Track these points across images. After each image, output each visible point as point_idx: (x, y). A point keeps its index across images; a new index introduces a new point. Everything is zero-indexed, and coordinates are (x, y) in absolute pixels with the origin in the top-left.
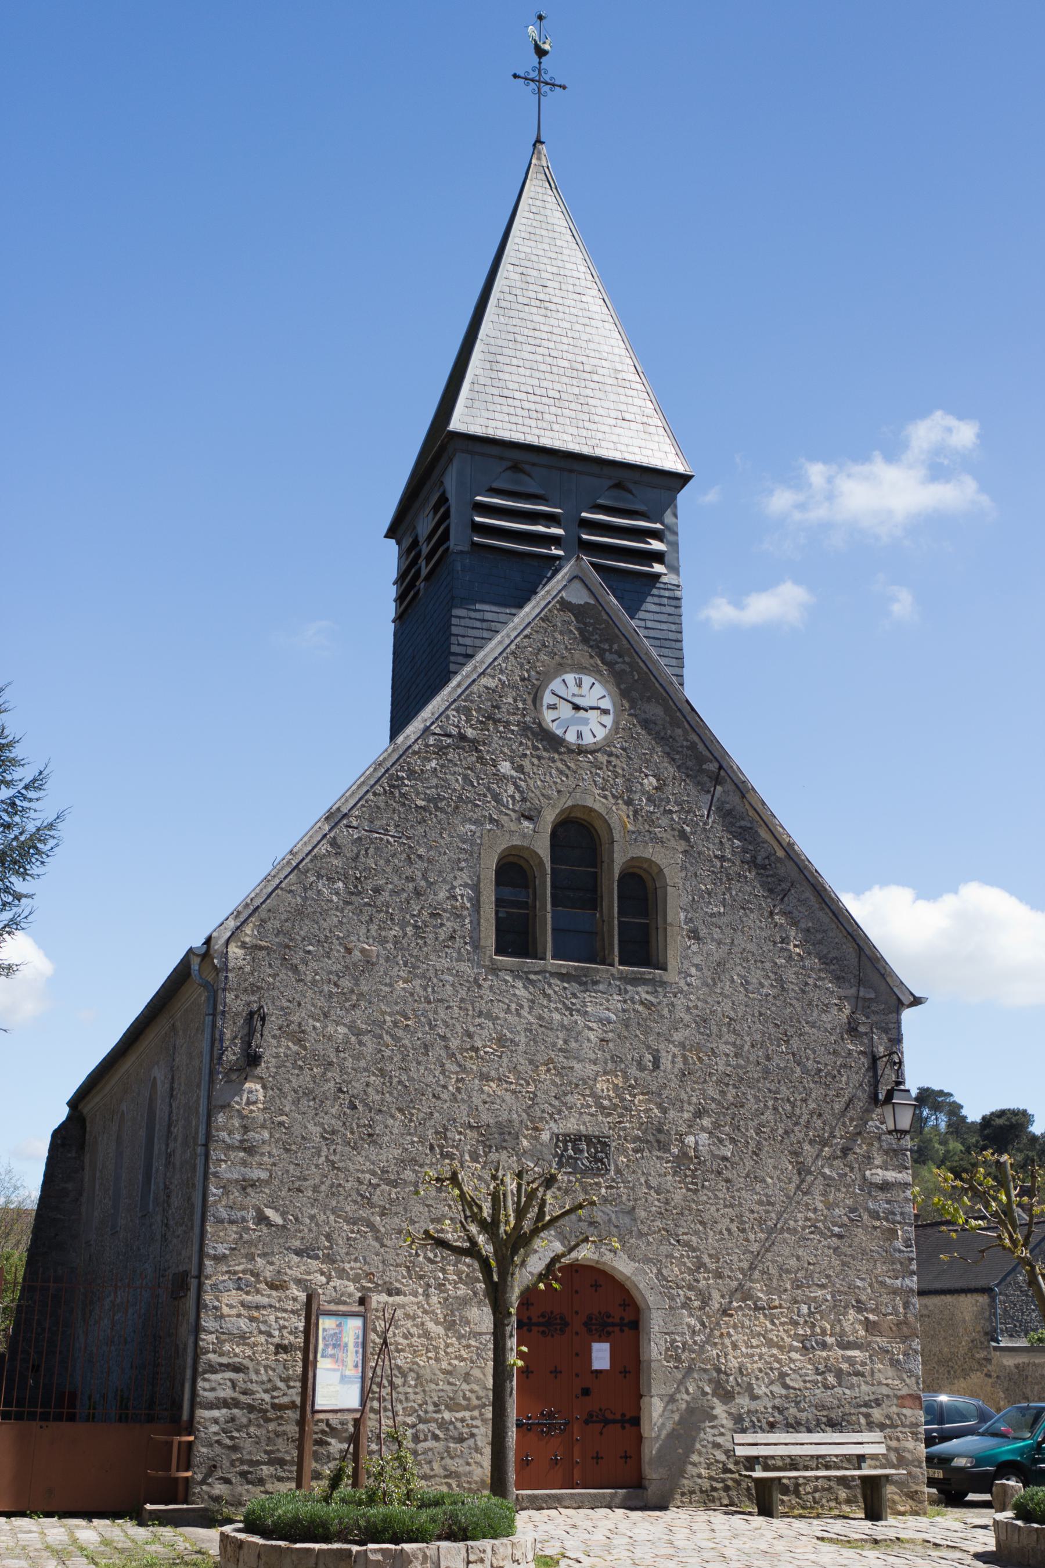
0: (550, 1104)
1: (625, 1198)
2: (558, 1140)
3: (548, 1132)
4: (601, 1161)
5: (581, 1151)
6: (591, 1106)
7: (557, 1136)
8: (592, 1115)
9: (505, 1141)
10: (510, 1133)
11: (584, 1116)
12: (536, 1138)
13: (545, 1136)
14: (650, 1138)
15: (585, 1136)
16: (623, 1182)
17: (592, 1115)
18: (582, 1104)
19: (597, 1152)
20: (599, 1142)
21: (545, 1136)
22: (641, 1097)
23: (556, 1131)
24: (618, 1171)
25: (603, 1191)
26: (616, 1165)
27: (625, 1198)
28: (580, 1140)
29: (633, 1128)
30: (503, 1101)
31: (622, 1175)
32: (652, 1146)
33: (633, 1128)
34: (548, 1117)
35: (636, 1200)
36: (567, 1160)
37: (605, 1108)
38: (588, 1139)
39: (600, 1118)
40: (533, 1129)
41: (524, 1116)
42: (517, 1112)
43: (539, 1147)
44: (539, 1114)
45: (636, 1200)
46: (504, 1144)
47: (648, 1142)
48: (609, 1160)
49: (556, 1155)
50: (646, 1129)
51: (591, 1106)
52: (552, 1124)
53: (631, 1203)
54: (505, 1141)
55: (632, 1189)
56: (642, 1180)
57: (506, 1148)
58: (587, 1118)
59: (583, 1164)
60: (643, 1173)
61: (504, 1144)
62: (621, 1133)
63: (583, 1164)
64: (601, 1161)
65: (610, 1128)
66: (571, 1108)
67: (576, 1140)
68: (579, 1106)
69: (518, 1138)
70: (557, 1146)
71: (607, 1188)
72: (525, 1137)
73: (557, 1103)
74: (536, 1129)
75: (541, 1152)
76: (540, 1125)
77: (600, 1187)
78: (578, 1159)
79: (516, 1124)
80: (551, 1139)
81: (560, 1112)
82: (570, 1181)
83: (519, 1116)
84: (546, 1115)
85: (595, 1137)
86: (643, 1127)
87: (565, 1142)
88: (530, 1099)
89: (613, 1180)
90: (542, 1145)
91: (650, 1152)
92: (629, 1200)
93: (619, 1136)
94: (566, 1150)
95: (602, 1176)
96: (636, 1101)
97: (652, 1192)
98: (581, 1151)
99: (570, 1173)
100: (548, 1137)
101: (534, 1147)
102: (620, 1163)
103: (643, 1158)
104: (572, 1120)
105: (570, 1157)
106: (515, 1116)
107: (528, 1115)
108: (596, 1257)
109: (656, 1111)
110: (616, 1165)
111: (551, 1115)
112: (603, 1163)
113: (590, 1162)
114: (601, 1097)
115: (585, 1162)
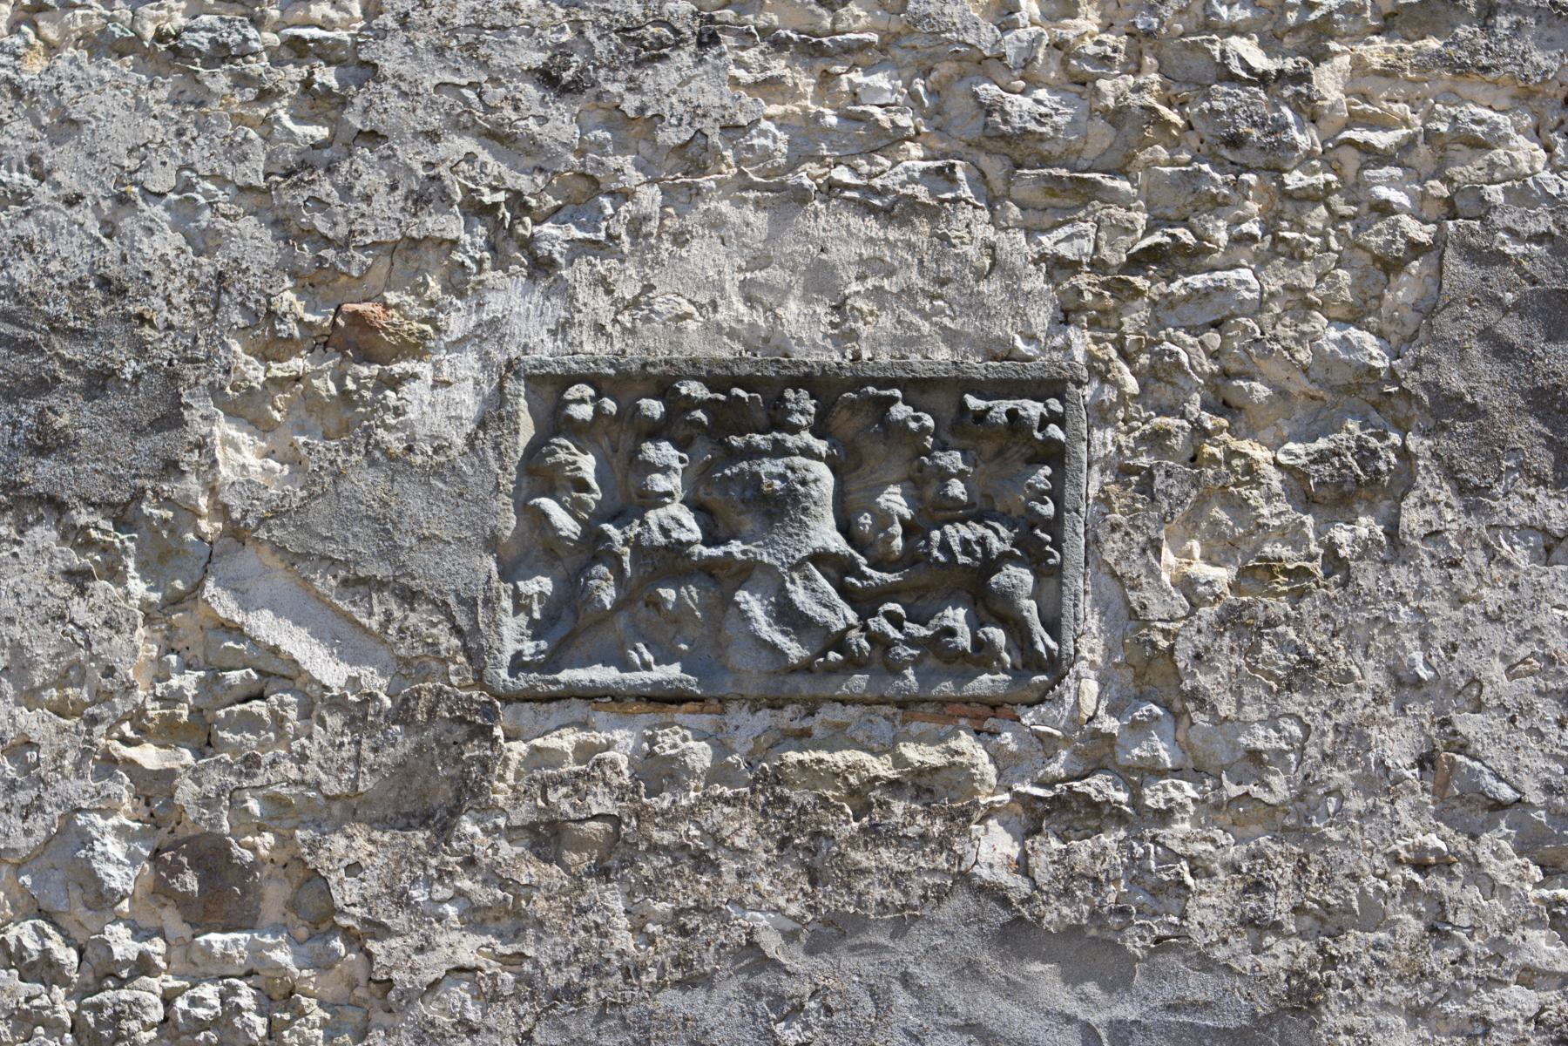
0: (498, 137)
1: (1209, 908)
2: (555, 422)
3: (467, 363)
4: (975, 585)
5: (780, 507)
6: (893, 140)
7: (550, 386)
8: (897, 211)
9: (47, 443)
10: (100, 381)
11: (822, 221)
12: (347, 417)
13: (439, 400)
14: (1473, 376)
15: (820, 383)
16: (1197, 772)
17: (897, 211)
18: (805, 132)
19: (933, 510)
20: (964, 428)
21: (439, 400)
22: (1377, 51)
23: (545, 350)
24: (1147, 672)
25: (993, 848)
26: (1129, 619)
27: (1209, 908)
28: (778, 420)
29: (1301, 304)
30: (67, 126)
31: (1181, 703)
32: (1492, 448)
33: (1301, 304)
34: (472, 240)
35: (1327, 922)
36: (635, 594)
37: (1018, 147)
38: (852, 408)
39: (973, 228)
40: (322, 342)
41: (252, 241)
42: (184, 211)
43: (366, 482)
44: (384, 216)
45: (1327, 922)
46: (42, 473)
47: (1447, 408)
48: (1048, 574)
49: (540, 545)
50: (1428, 310)
51: (893, 140)
52: (509, 295)
53: (1280, 954)
54: (47, 443)
55: (1295, 823)
56: (1396, 745)
57: (56, 506)
58: (846, 237)
59: (786, 614)
60: (1404, 683)
61: (42, 473)
62: (1187, 349)
63: (786, 614)
64: (975, 585)
65: (1066, 316)
66: (694, 156)
67: (728, 417)
68: (777, 142)
69: (172, 419)
70: (540, 473)
71: (1032, 819)
72: (246, 408)
73: (559, 124)
74: (355, 340)
75: (384, 527)
76: (396, 309)
77: (962, 818)
78: (746, 573)
79: (169, 307)
80: (494, 415)
81: (584, 193)
82: (659, 771)
83: (204, 241)
84: (452, 225)
85: (918, 388)
86: (1402, 293)
87: (622, 438)
88: (314, 101)
89: (1098, 753)
90: (395, 464)
91: (1471, 495)
92: (1258, 926)
93: (1161, 374)
94: (632, 502)
95: (985, 715)
96: (1329, 83)
97: (1498, 851)
98: (780, 507)
99: (664, 699)
100: (468, 402)
101: (320, 483)
102: (1161, 604)
103: (1395, 545)
104: (703, 254)
105: (669, 561)
106: (168, 242)
107: (284, 227)
108: (385, 944)
109: (1525, 152)
110: (1129, 619)
111: (502, 225)
112: (991, 606)
113: (865, 602)
114: (985, 64)
115: (815, 598)
